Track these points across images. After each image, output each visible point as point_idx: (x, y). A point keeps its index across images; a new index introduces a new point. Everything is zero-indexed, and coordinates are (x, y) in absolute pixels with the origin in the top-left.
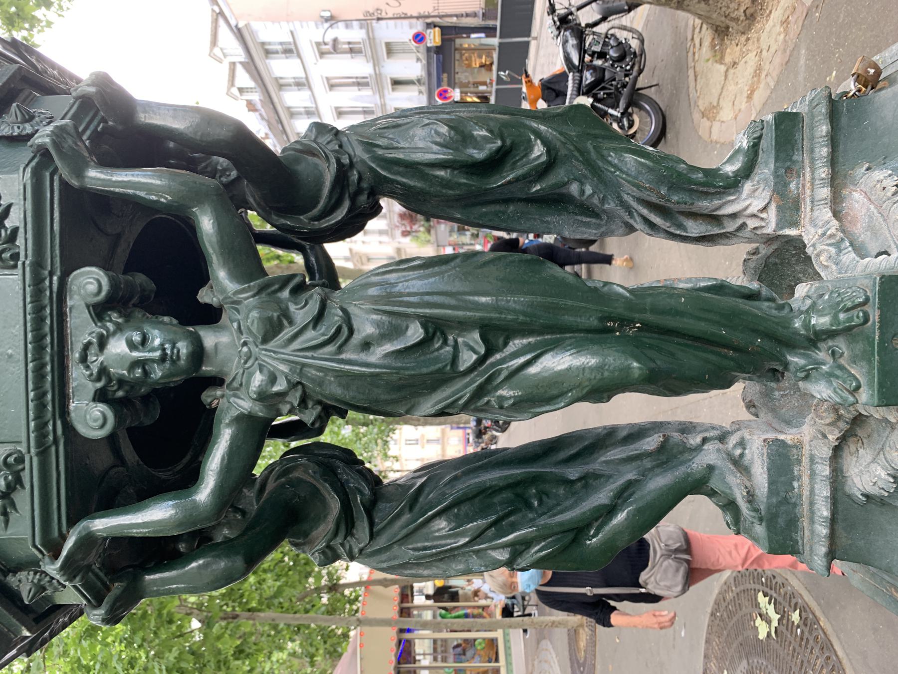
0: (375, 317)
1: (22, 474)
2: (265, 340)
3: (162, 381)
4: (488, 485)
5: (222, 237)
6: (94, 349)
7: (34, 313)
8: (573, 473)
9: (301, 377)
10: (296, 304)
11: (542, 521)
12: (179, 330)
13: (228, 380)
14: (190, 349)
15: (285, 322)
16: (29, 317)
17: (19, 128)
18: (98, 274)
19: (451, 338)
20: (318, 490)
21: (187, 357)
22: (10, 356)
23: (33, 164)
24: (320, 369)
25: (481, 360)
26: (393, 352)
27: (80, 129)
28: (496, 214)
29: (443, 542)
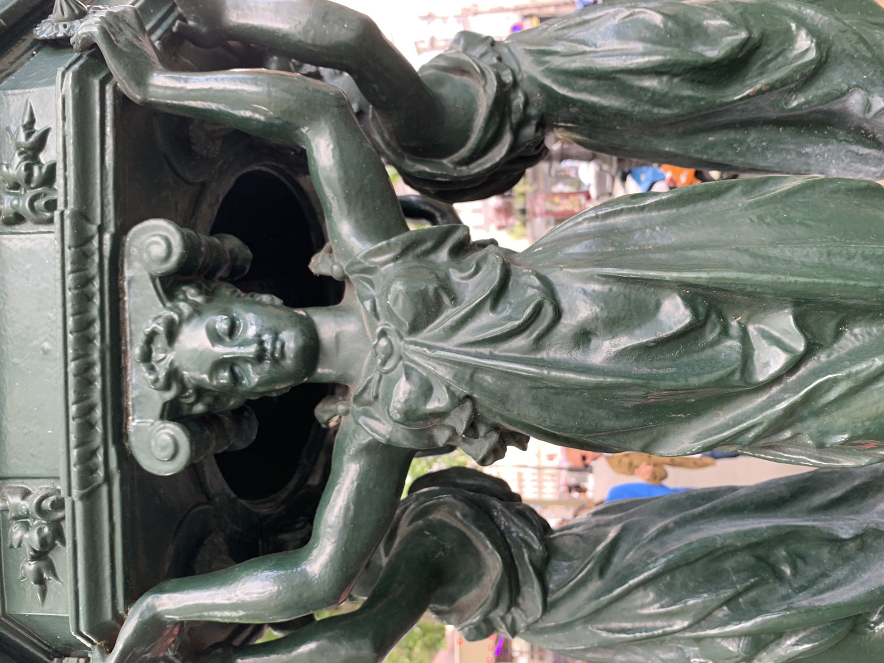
0: (597, 287)
1: (62, 523)
2: (415, 328)
3: (261, 389)
4: (719, 543)
5: (346, 172)
6: (161, 342)
7: (76, 288)
8: (845, 526)
9: (472, 388)
10: (461, 270)
11: (804, 601)
12: (285, 313)
13: (354, 391)
14: (301, 342)
15: (446, 300)
16: (69, 294)
17: (65, 26)
18: (167, 230)
19: (734, 323)
20: (468, 540)
21: (296, 356)
22: (46, 352)
23: (76, 66)
24: (507, 375)
25: (792, 367)
26: (634, 348)
27: (148, 27)
28: (730, 145)
29: (649, 624)
